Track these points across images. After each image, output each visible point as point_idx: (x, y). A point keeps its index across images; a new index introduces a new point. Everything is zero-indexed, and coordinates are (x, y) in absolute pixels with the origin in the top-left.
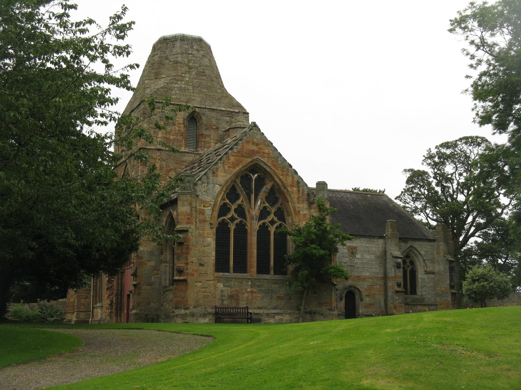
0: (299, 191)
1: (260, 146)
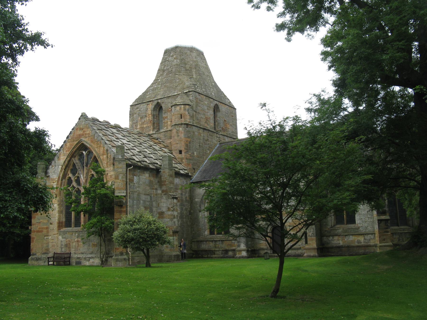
0: (107, 157)
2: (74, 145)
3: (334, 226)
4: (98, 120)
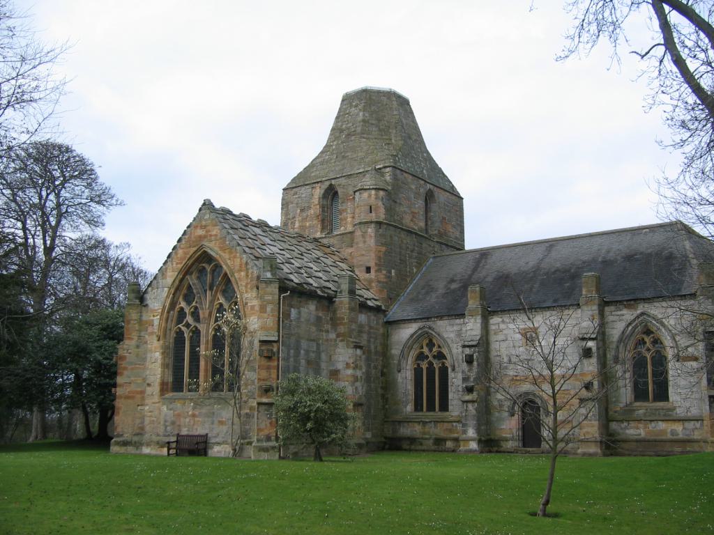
0: (247, 276)
1: (208, 228)
2: (190, 254)
3: (631, 403)
4: (230, 213)
